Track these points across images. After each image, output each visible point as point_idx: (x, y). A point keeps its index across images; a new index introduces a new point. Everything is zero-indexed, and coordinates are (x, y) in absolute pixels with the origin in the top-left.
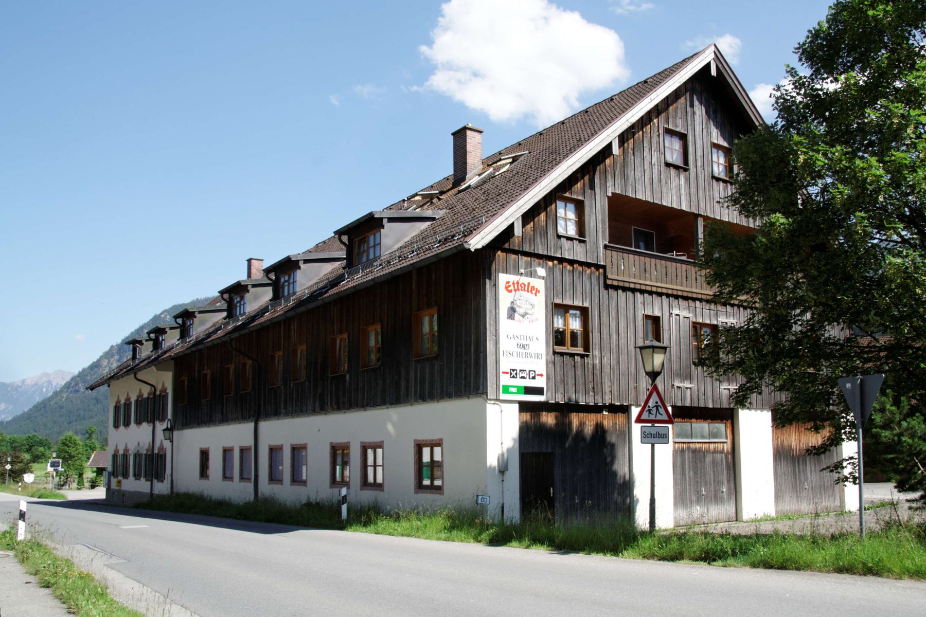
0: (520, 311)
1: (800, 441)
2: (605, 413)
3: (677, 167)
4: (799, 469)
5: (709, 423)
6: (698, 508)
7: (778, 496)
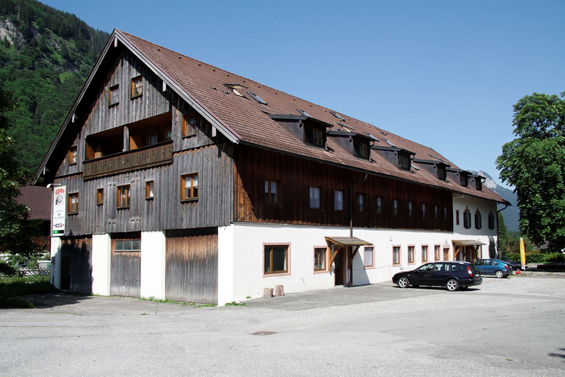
0: (59, 200)
1: (189, 250)
2: (86, 239)
3: (109, 103)
4: (187, 270)
5: (190, 244)
6: (124, 287)
7: (168, 287)
